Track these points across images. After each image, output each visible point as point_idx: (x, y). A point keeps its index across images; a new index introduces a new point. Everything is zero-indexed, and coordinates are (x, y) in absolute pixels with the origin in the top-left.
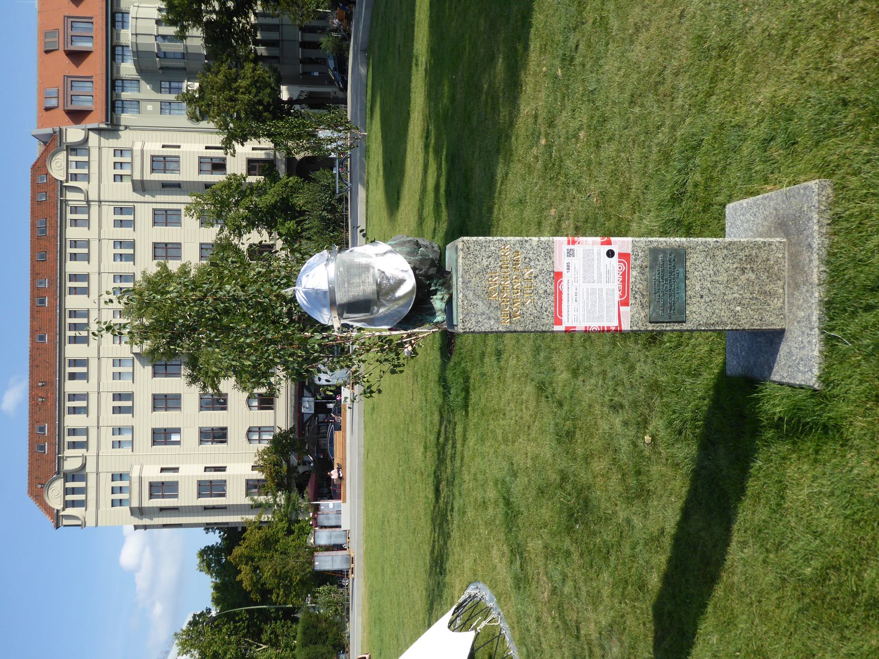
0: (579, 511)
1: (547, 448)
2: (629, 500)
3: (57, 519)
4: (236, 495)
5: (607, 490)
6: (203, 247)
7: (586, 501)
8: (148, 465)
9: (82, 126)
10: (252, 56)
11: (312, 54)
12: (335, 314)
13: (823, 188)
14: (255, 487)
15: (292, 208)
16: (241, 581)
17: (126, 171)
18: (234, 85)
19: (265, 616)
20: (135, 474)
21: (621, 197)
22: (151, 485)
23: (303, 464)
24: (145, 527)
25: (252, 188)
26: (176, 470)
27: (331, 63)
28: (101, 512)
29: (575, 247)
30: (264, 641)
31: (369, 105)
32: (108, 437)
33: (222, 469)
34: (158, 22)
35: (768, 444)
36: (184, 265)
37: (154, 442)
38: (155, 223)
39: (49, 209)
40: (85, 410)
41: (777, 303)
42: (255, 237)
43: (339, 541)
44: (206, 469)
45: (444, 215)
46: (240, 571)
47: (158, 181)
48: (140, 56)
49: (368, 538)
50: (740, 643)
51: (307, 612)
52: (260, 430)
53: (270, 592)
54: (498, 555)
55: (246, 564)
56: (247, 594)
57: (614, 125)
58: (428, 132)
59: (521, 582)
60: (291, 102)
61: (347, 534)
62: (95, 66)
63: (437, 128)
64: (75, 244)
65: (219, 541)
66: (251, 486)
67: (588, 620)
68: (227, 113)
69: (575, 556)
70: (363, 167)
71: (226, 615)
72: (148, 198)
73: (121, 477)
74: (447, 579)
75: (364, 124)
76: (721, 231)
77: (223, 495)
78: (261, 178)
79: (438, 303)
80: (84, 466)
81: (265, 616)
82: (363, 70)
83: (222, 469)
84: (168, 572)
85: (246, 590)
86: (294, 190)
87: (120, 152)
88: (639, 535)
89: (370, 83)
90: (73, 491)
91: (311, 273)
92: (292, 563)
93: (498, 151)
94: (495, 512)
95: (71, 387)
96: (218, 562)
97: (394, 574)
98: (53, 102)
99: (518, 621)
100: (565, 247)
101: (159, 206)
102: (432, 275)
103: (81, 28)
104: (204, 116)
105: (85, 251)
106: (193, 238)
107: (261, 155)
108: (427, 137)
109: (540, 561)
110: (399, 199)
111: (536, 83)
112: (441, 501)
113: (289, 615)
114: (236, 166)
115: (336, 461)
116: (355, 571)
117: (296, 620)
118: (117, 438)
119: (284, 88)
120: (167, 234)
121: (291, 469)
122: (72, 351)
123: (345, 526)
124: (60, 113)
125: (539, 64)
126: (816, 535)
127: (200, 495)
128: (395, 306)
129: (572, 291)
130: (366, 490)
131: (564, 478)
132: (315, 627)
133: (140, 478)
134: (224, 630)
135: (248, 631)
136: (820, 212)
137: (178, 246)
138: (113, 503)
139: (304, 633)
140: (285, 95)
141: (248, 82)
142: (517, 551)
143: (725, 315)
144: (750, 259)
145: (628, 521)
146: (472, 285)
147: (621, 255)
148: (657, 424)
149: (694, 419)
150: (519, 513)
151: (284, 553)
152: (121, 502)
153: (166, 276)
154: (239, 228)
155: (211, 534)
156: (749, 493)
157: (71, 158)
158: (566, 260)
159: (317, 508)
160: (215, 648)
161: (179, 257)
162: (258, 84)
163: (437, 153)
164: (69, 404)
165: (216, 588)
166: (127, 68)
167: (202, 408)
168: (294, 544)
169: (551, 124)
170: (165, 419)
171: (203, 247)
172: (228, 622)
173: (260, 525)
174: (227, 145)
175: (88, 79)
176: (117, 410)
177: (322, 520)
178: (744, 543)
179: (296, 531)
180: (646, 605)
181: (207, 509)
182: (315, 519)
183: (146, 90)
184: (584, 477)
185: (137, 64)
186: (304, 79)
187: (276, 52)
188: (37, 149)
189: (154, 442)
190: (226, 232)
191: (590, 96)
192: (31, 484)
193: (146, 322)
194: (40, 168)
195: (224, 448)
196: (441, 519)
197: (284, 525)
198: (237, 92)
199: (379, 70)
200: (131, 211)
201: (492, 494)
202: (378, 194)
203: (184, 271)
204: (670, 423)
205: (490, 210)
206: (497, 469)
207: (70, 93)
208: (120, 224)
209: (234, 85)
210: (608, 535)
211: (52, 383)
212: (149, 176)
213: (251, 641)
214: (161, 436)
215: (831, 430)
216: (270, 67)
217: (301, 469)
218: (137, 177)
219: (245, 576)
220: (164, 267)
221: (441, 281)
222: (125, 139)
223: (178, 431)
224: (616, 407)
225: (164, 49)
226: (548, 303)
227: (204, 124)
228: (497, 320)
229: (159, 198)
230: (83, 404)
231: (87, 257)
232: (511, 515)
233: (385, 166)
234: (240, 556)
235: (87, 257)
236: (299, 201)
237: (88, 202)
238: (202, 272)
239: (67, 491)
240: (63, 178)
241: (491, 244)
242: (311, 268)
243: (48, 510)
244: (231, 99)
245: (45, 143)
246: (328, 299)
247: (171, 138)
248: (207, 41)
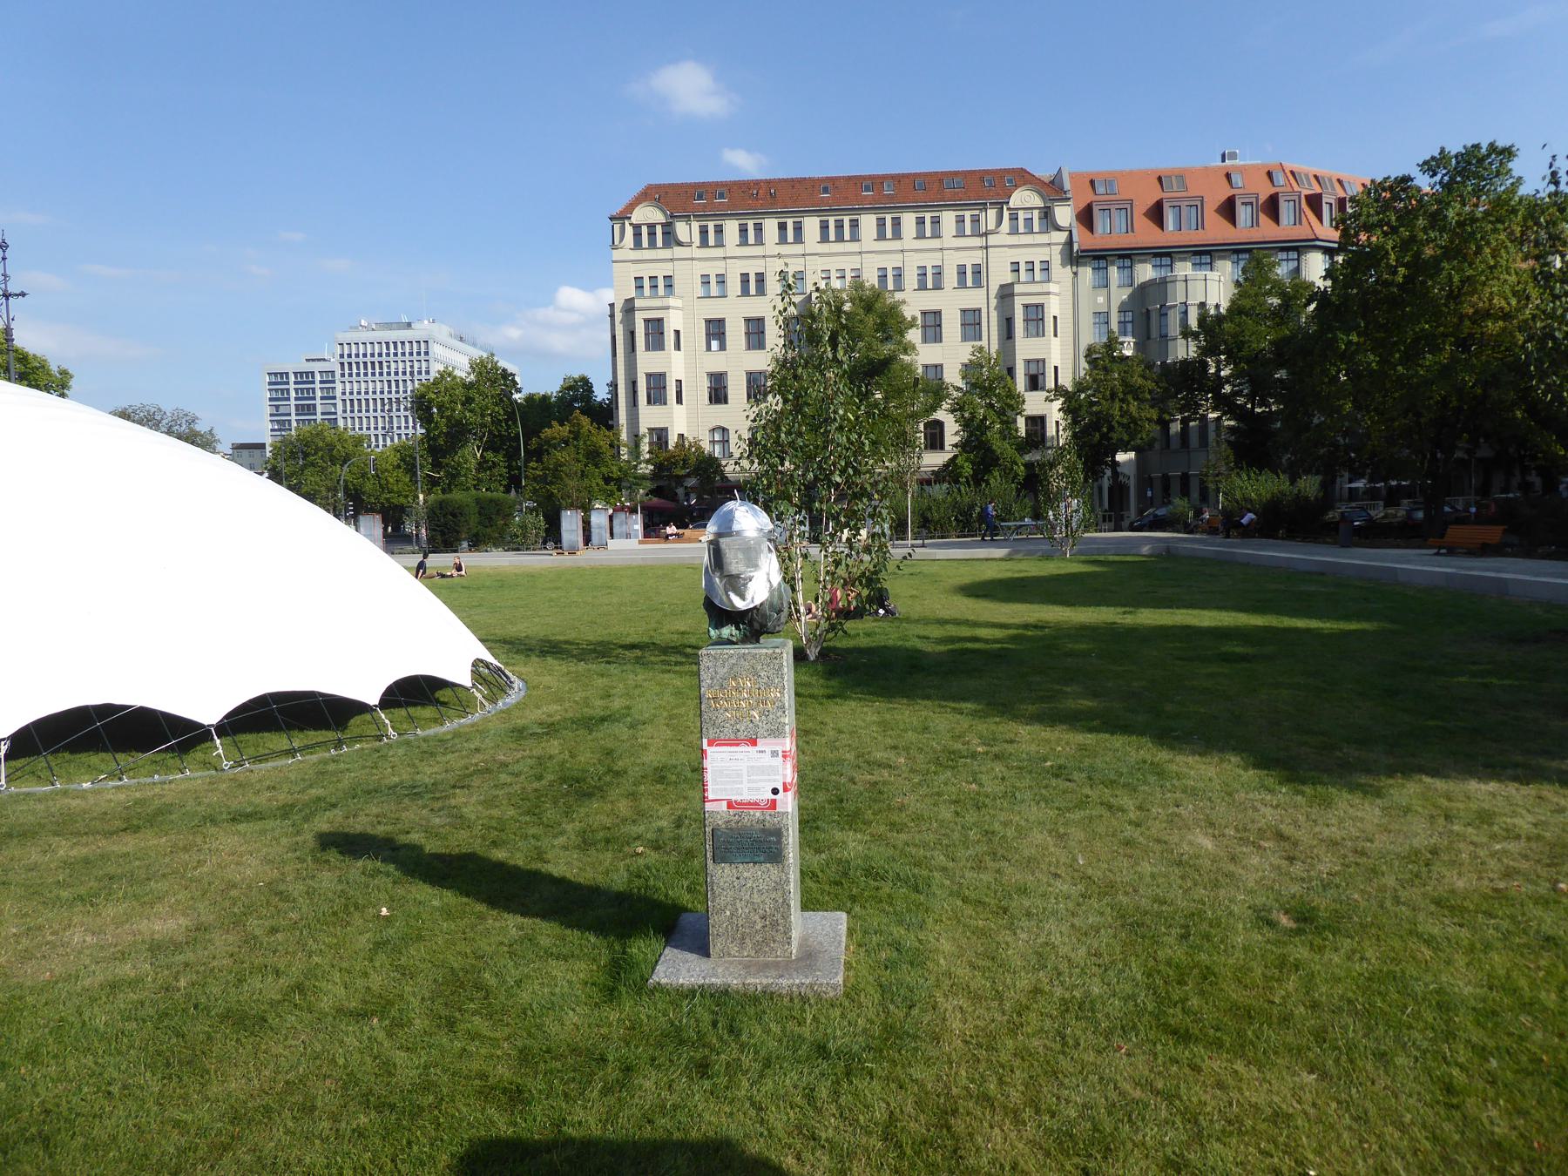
0: (580, 788)
1: (651, 758)
2: (582, 833)
3: (621, 217)
4: (650, 416)
5: (596, 813)
6: (938, 368)
7: (590, 795)
8: (682, 315)
9: (1075, 223)
10: (1167, 417)
11: (1175, 487)
12: (711, 537)
13: (835, 988)
14: (659, 438)
15: (988, 471)
16: (551, 427)
17: (1023, 276)
18: (1130, 398)
19: (512, 455)
20: (671, 301)
21: (892, 825)
22: (660, 320)
23: (682, 491)
24: (612, 316)
25: (1009, 424)
26: (678, 347)
27: (1161, 512)
28: (629, 265)
29: (780, 758)
31: (1102, 558)
32: (713, 269)
33: (679, 400)
34: (1202, 305)
35: (610, 947)
36: (914, 348)
37: (708, 322)
38: (964, 311)
39: (980, 191)
40: (744, 242)
41: (734, 949)
42: (952, 432)
44: (679, 382)
45: (942, 648)
46: (562, 425)
47: (1014, 313)
48: (1161, 285)
49: (596, 571)
50: (428, 924)
51: (515, 503)
52: (725, 442)
54: (554, 710)
56: (537, 433)
57: (971, 817)
58: (1043, 627)
59: (519, 733)
60: (1115, 464)
62: (1146, 234)
63: (1042, 638)
64: (936, 222)
66: (660, 435)
67: (471, 795)
68: (1097, 390)
69: (536, 785)
70: (1030, 553)
71: (513, 412)
72: (993, 302)
73: (669, 286)
74: (534, 659)
75: (1081, 553)
76: (809, 904)
77: (649, 402)
78: (1022, 432)
79: (727, 631)
80: (680, 244)
81: (512, 455)
82: (1145, 550)
83: (679, 400)
84: (558, 342)
86: (1008, 473)
87: (1046, 267)
88: (544, 843)
89: (1128, 559)
90: (652, 234)
91: (749, 515)
92: (572, 483)
93: (988, 704)
94: (598, 707)
95: (771, 226)
96: (575, 399)
97: (551, 600)
98: (1101, 190)
99: (480, 730)
100: (780, 749)
101: (984, 315)
102: (754, 625)
103: (1189, 215)
104: (1093, 363)
105: (928, 234)
106: (948, 357)
107: (1051, 431)
108: (1036, 627)
109: (537, 752)
110: (977, 596)
111: (1048, 741)
113: (514, 482)
114: (1035, 403)
115: (687, 532)
117: (508, 491)
118: (713, 280)
119: (1132, 455)
120: (952, 326)
121: (680, 480)
122: (811, 225)
123: (613, 544)
124: (1090, 197)
125: (1063, 742)
126: (518, 983)
127: (649, 376)
128: (721, 591)
129: (738, 756)
130: (652, 567)
131: (617, 774)
132: (498, 513)
133: (667, 308)
136: (811, 986)
137: (938, 338)
138: (639, 279)
139: (491, 501)
140: (1121, 457)
141: (1135, 414)
142: (551, 729)
143: (721, 901)
144: (774, 925)
145: (562, 833)
147: (774, 801)
148: (653, 857)
149: (647, 887)
150: (591, 731)
151: (583, 475)
152: (640, 287)
153: (903, 325)
154: (961, 409)
155: (607, 389)
156: (568, 932)
157: (1036, 213)
158: (768, 749)
159: (633, 511)
160: (478, 398)
161: (925, 341)
162: (1133, 425)
163: (1013, 639)
164: (751, 224)
165: (545, 398)
166: (1146, 272)
167: (749, 374)
169: (997, 757)
170: (736, 333)
171: (938, 368)
172: (506, 413)
173: (615, 446)
174: (1059, 391)
175: (1130, 227)
176: (745, 278)
177: (621, 517)
178: (521, 928)
180: (477, 847)
181: (633, 384)
182: (622, 509)
183: (1121, 295)
184: (614, 793)
185: (1152, 282)
186: (1144, 479)
187: (1175, 444)
188: (1045, 173)
189: (708, 322)
190: (955, 394)
191: (1010, 796)
192: (659, 187)
193: (847, 307)
194: (1022, 177)
195: (699, 403)
196: (602, 651)
197: (616, 474)
198: (1122, 401)
199: (1142, 570)
200: (978, 284)
201: (617, 704)
202: (991, 573)
203: (908, 348)
204: (648, 868)
205: (928, 698)
206: (643, 708)
207: (1113, 208)
208: (962, 271)
209: (1130, 398)
210: (550, 814)
211: (773, 205)
212: (1019, 303)
214: (716, 330)
215: (610, 994)
216: (1154, 440)
217: (680, 491)
218: (1018, 289)
219: (557, 431)
220: (912, 324)
222: (1062, 273)
223: (722, 347)
224: (678, 824)
225: (1171, 313)
226: (728, 733)
227: (1084, 365)
228: (710, 686)
229: (994, 315)
230: (751, 239)
231: (921, 236)
232: (589, 724)
233: (1022, 579)
235: (921, 236)
236: (995, 479)
237: (986, 234)
238: (909, 368)
239: (652, 226)
240: (1011, 205)
242: (755, 514)
243: (631, 207)
244: (1113, 396)
245: (1052, 182)
246: (726, 531)
247: (1065, 326)
248: (1184, 362)
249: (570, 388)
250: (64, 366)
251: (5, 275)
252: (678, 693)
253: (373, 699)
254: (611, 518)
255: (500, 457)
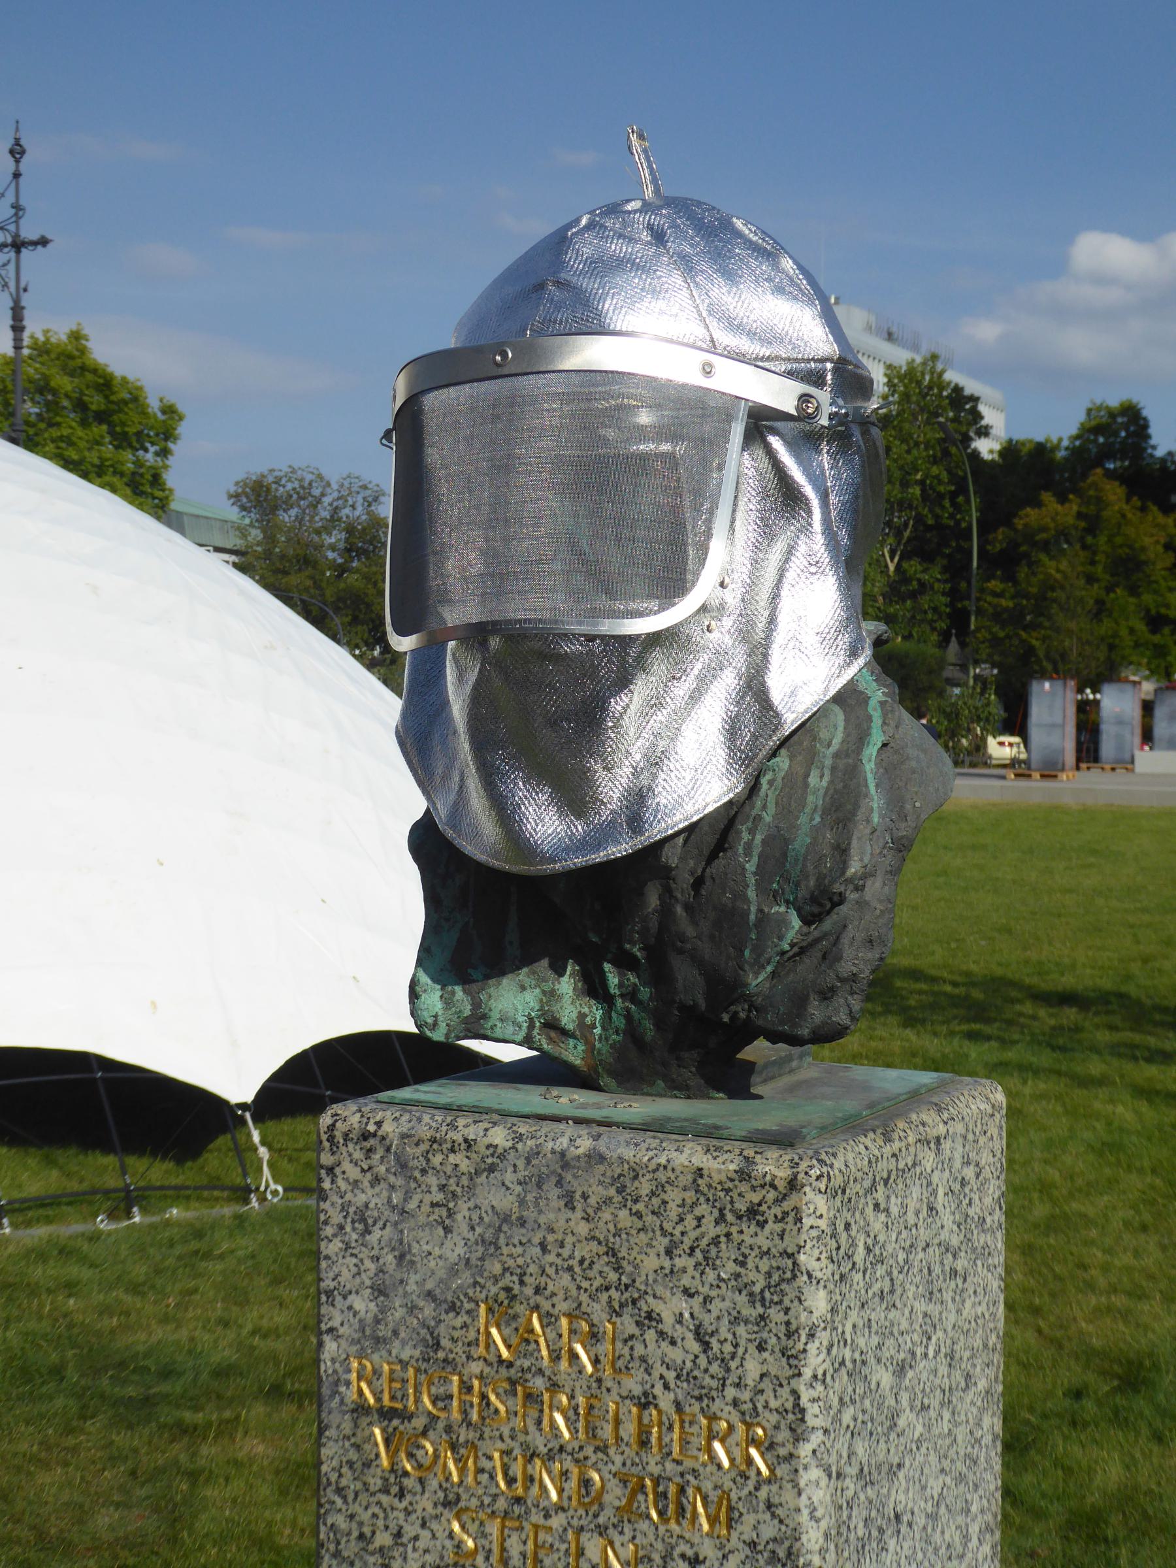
16: (1039, 504)
19: (957, 570)
30: (905, 565)
43: (1107, 748)
46: (1062, 499)
53: (1010, 577)
55: (1080, 515)
56: (1007, 520)
61: (1128, 763)
65: (1160, 453)
81: (957, 570)
85: (1015, 515)
96: (1106, 453)
112: (1028, 1008)
116: (1023, 783)
117: (944, 642)
123: (1148, 761)
134: (935, 470)
135: (929, 528)
146: (553, 1213)
168: (1124, 632)
179: (1156, 639)
213: (907, 534)
219: (1052, 512)
221: (648, 1028)
228: (372, 1337)
234: (1099, 500)
241: (778, 1366)
249: (1097, 430)
250: (171, 399)
251: (17, 207)
252: (1110, 1148)
253: (239, 1086)
254: (1148, 708)
255: (936, 572)
